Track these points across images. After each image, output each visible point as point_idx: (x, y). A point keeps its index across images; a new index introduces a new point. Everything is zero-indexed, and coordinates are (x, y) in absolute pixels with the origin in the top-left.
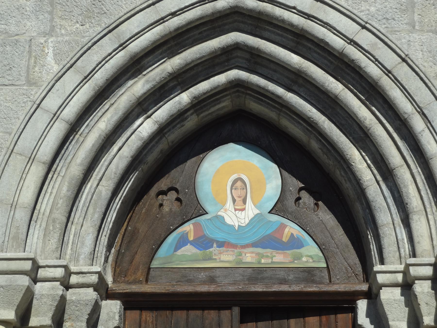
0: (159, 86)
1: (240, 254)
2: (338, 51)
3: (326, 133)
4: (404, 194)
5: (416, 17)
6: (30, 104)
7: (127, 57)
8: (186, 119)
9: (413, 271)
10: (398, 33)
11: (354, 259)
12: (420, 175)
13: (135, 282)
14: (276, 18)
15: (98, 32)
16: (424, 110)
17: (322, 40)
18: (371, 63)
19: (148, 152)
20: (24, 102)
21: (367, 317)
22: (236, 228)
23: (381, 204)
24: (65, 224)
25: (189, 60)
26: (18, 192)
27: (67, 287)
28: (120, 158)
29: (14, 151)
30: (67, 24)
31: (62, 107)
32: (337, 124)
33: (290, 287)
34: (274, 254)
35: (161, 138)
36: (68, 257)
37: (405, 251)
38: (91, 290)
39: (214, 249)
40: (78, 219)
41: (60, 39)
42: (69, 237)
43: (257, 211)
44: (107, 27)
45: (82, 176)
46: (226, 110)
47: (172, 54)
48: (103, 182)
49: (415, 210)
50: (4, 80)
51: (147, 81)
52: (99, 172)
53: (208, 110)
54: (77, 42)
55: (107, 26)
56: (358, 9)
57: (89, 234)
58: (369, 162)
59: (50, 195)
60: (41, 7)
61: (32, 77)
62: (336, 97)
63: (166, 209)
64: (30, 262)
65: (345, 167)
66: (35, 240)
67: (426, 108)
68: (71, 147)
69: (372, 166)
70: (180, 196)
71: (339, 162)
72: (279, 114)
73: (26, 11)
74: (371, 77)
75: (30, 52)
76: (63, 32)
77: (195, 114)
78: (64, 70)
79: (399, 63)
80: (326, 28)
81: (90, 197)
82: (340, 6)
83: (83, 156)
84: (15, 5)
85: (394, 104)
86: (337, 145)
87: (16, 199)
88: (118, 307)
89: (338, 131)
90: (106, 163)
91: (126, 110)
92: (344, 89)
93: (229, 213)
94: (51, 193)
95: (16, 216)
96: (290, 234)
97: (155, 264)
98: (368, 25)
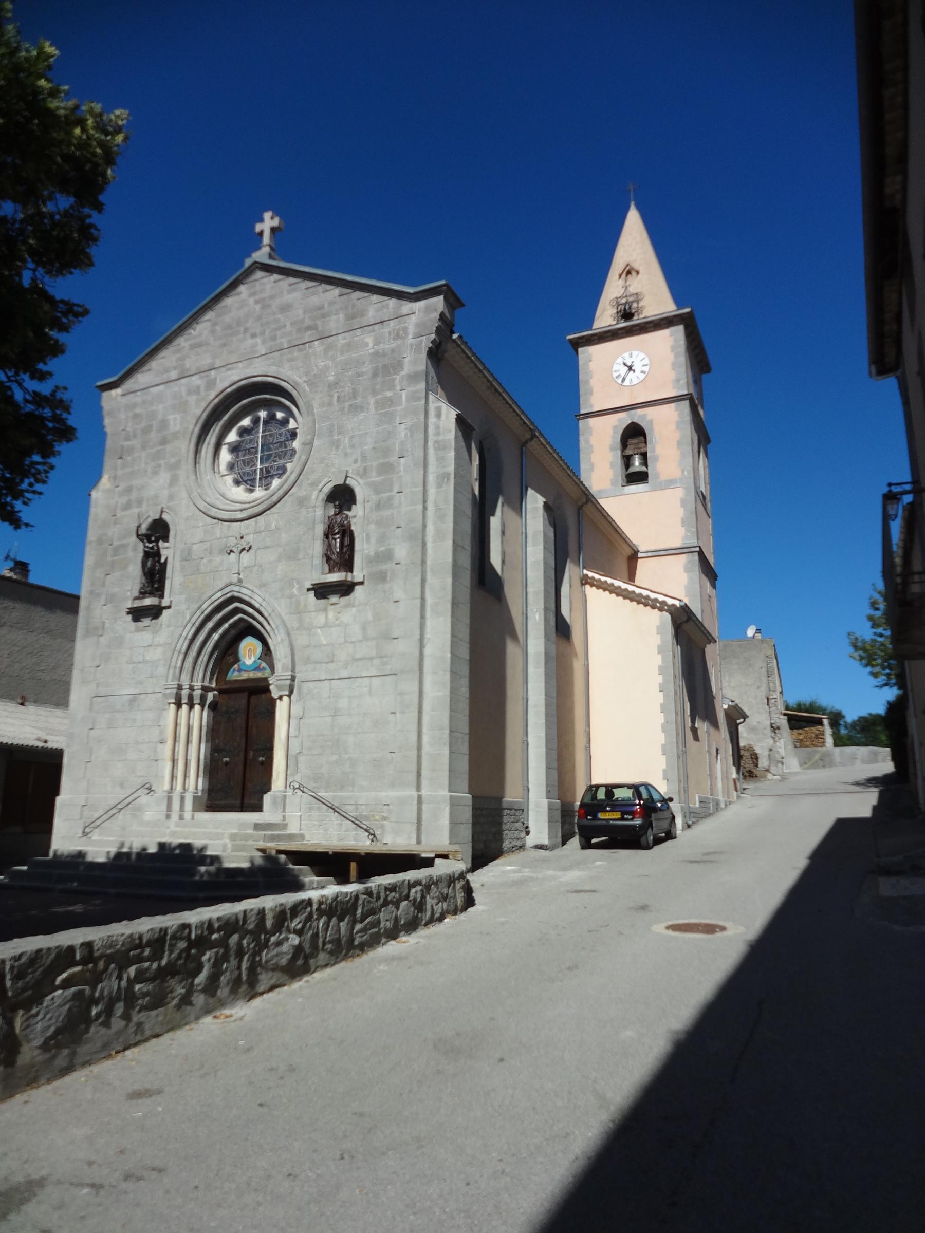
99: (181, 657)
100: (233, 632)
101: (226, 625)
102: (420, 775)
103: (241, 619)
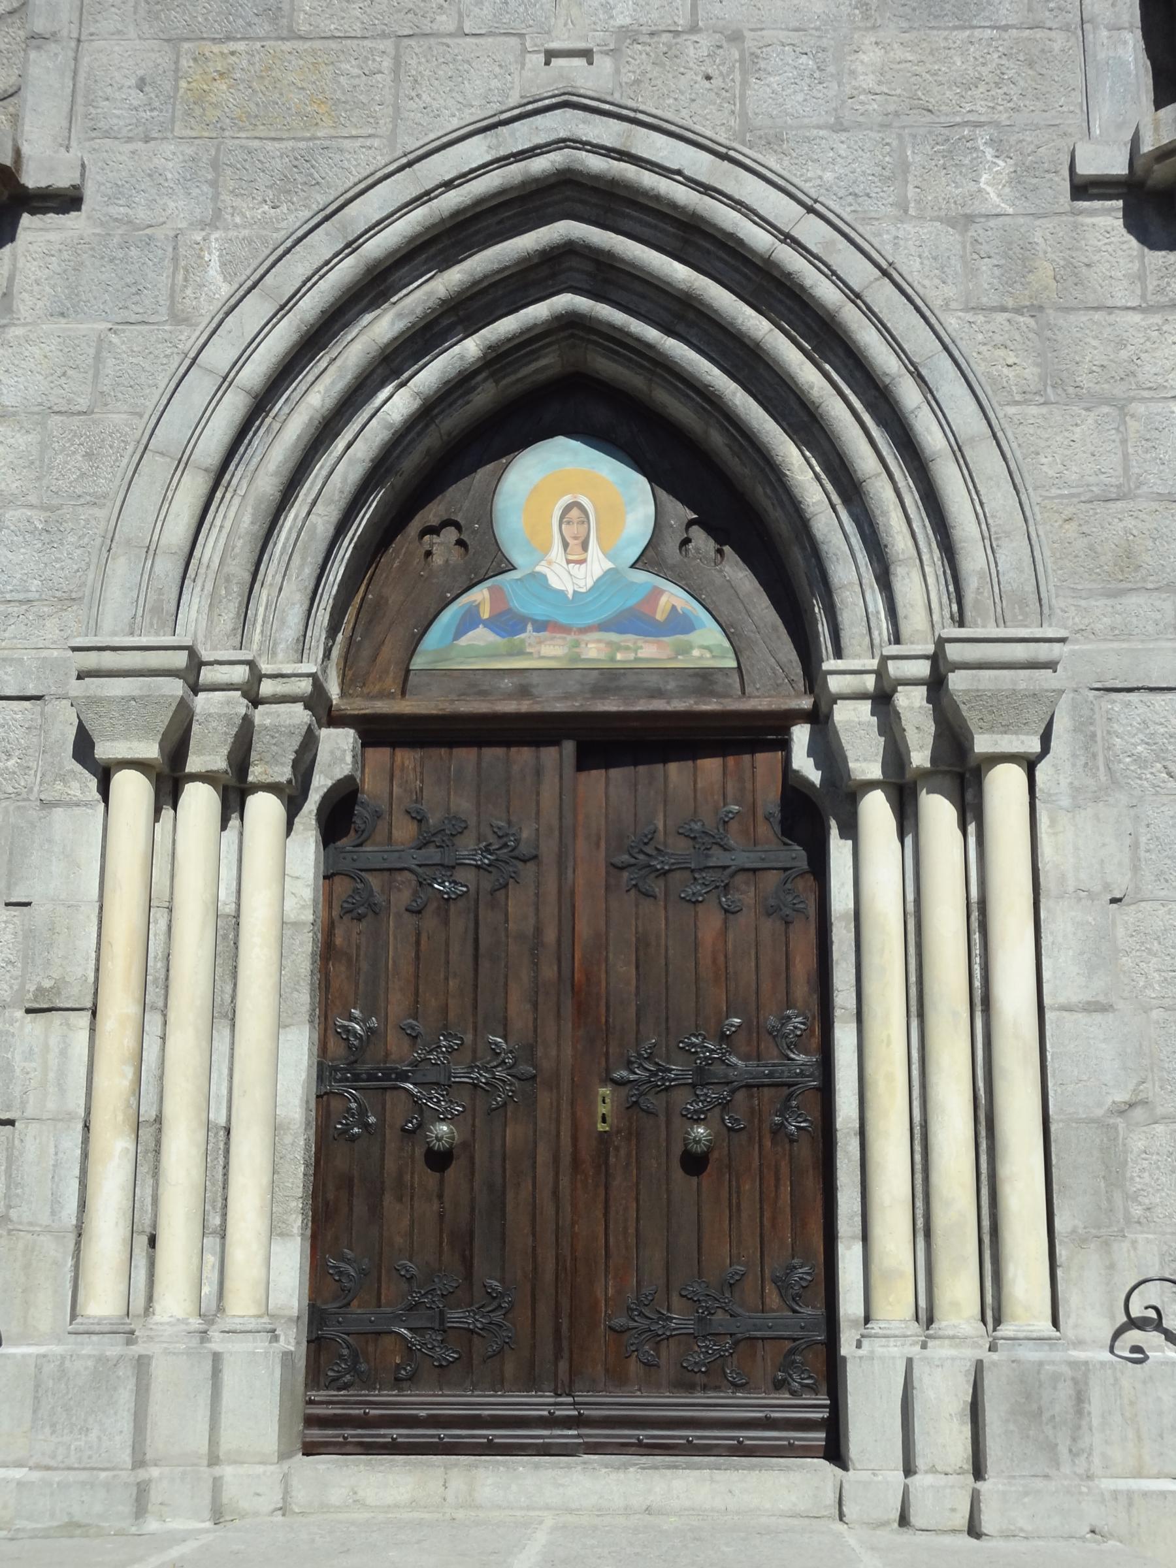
0: (422, 324)
1: (577, 644)
2: (761, 257)
3: (738, 416)
4: (882, 528)
5: (911, 192)
6: (177, 360)
7: (362, 267)
8: (474, 388)
9: (893, 668)
10: (876, 223)
11: (788, 652)
12: (912, 492)
13: (383, 695)
14: (645, 193)
15: (304, 220)
16: (920, 369)
17: (732, 236)
18: (823, 278)
19: (402, 452)
20: (166, 356)
21: (809, 756)
22: (570, 596)
23: (839, 548)
24: (248, 586)
25: (479, 274)
26: (159, 524)
27: (256, 701)
28: (351, 462)
29: (150, 447)
30: (245, 205)
31: (238, 363)
32: (760, 397)
33: (668, 703)
34: (640, 644)
35: (427, 426)
36: (255, 646)
37: (880, 634)
38: (299, 707)
39: (528, 635)
40: (274, 577)
41: (232, 234)
42: (257, 610)
43: (609, 565)
44: (322, 210)
45: (278, 495)
46: (550, 373)
47: (446, 263)
48: (320, 507)
49: (901, 557)
50: (126, 313)
51: (400, 316)
52: (310, 488)
53: (515, 372)
54: (265, 242)
55: (321, 207)
56: (802, 175)
57: (293, 604)
58: (818, 469)
59: (220, 531)
60: (195, 173)
61: (180, 307)
62: (758, 344)
63: (438, 560)
64: (184, 654)
65: (773, 478)
66: (193, 614)
67: (925, 365)
68: (257, 441)
69: (823, 476)
70: (464, 537)
71: (762, 470)
72: (650, 380)
73: (166, 180)
74: (823, 307)
75: (175, 260)
76: (238, 220)
77: (491, 380)
78: (241, 292)
79: (877, 279)
80: (739, 211)
81: (294, 536)
82: (767, 168)
83: (280, 458)
84: (144, 167)
85: (866, 358)
86: (758, 438)
87: (155, 538)
88: (351, 740)
89: (761, 411)
90: (324, 473)
91: (359, 370)
92: (771, 330)
93: (555, 567)
94: (221, 527)
95: (156, 569)
96: (669, 607)
97: (418, 663)
98: (818, 206)
99: (192, 487)
100: (484, 397)
101: (470, 348)
102: (136, 1414)
103: (570, 323)
